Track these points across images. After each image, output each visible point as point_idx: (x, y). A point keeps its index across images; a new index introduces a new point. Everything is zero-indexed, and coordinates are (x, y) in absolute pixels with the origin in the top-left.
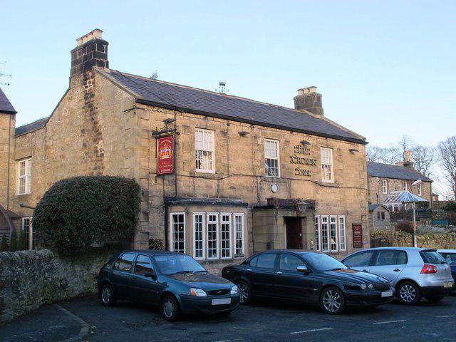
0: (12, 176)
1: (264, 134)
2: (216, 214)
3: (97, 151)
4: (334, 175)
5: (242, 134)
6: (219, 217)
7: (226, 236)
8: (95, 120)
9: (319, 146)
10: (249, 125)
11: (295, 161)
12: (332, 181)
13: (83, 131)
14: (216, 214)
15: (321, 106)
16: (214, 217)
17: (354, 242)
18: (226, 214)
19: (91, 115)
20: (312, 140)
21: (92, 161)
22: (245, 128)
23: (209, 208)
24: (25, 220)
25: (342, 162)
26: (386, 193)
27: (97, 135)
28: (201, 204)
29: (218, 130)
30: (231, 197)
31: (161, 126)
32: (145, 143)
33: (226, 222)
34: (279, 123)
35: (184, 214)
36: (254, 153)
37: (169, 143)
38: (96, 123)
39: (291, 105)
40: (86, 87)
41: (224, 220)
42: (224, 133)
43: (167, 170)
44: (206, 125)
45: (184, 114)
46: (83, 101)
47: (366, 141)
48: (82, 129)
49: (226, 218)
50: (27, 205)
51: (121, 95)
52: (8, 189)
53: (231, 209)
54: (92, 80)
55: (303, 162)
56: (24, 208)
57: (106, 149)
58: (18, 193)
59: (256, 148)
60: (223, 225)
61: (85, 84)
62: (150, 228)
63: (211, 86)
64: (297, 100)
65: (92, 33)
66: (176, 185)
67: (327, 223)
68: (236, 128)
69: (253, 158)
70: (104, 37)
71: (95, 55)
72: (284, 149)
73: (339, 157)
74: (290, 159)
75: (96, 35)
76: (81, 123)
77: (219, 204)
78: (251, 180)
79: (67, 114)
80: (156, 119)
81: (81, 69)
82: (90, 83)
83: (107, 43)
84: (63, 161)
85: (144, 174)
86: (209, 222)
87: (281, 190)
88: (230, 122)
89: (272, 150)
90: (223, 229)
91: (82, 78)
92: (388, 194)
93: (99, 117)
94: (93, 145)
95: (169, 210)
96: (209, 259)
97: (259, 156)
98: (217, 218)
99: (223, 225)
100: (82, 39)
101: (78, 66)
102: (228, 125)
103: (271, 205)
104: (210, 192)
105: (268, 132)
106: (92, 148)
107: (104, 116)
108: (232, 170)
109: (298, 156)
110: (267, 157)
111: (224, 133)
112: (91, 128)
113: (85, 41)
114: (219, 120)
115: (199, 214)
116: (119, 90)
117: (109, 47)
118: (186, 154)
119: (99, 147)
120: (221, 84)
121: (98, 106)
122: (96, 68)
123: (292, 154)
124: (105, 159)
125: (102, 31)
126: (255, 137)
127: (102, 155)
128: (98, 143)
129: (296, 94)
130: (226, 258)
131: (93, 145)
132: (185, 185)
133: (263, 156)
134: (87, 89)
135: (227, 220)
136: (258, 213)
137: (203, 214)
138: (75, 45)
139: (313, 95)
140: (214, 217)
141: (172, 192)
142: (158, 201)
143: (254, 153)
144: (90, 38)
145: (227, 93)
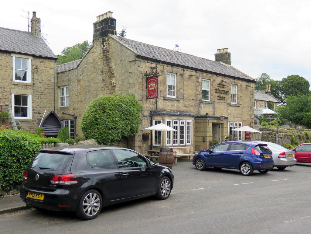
0: (56, 95)
1: (202, 76)
2: (178, 121)
3: (111, 84)
4: (238, 99)
5: (191, 76)
7: (182, 132)
8: (110, 66)
9: (230, 83)
10: (194, 71)
11: (218, 91)
13: (102, 72)
15: (230, 60)
16: (177, 122)
17: (246, 137)
18: (182, 121)
19: (107, 63)
20: (227, 80)
21: (108, 90)
22: (193, 73)
23: (174, 118)
24: (65, 121)
27: (111, 74)
28: (170, 115)
29: (178, 74)
30: (184, 112)
31: (148, 71)
32: (140, 80)
33: (182, 125)
34: (210, 70)
35: (161, 120)
37: (154, 81)
38: (110, 68)
39: (213, 58)
40: (104, 46)
41: (175, 124)
42: (182, 75)
45: (161, 64)
46: (102, 55)
48: (101, 70)
49: (182, 123)
50: (67, 113)
51: (126, 52)
52: (54, 104)
53: (186, 118)
54: (107, 42)
56: (64, 115)
57: (117, 83)
58: (60, 106)
59: (198, 84)
61: (103, 44)
63: (170, 46)
64: (217, 56)
65: (106, 14)
66: (156, 104)
68: (187, 73)
69: (196, 90)
70: (114, 16)
71: (109, 27)
72: (212, 85)
73: (240, 90)
75: (109, 15)
76: (101, 67)
77: (180, 115)
78: (194, 102)
79: (91, 61)
80: (146, 67)
81: (100, 35)
82: (106, 44)
83: (115, 20)
84: (89, 89)
87: (210, 108)
88: (185, 69)
89: (205, 86)
91: (101, 40)
93: (113, 64)
94: (108, 80)
95: (153, 118)
97: (199, 89)
99: (181, 127)
100: (99, 16)
101: (98, 33)
102: (184, 71)
103: (206, 117)
104: (174, 108)
105: (204, 75)
106: (108, 82)
107: (116, 64)
108: (185, 96)
110: (203, 89)
111: (182, 75)
112: (107, 70)
113: (102, 18)
115: (169, 120)
116: (125, 49)
117: (116, 22)
118: (161, 87)
119: (113, 82)
120: (176, 46)
121: (111, 58)
122: (110, 35)
124: (117, 89)
125: (112, 13)
126: (198, 78)
127: (115, 86)
128: (112, 79)
129: (216, 52)
130: (175, 145)
131: (108, 80)
132: (161, 104)
134: (105, 47)
135: (177, 124)
136: (199, 121)
137: (171, 121)
138: (95, 20)
139: (226, 53)
140: (177, 122)
142: (147, 113)
144: (105, 17)
145: (179, 51)
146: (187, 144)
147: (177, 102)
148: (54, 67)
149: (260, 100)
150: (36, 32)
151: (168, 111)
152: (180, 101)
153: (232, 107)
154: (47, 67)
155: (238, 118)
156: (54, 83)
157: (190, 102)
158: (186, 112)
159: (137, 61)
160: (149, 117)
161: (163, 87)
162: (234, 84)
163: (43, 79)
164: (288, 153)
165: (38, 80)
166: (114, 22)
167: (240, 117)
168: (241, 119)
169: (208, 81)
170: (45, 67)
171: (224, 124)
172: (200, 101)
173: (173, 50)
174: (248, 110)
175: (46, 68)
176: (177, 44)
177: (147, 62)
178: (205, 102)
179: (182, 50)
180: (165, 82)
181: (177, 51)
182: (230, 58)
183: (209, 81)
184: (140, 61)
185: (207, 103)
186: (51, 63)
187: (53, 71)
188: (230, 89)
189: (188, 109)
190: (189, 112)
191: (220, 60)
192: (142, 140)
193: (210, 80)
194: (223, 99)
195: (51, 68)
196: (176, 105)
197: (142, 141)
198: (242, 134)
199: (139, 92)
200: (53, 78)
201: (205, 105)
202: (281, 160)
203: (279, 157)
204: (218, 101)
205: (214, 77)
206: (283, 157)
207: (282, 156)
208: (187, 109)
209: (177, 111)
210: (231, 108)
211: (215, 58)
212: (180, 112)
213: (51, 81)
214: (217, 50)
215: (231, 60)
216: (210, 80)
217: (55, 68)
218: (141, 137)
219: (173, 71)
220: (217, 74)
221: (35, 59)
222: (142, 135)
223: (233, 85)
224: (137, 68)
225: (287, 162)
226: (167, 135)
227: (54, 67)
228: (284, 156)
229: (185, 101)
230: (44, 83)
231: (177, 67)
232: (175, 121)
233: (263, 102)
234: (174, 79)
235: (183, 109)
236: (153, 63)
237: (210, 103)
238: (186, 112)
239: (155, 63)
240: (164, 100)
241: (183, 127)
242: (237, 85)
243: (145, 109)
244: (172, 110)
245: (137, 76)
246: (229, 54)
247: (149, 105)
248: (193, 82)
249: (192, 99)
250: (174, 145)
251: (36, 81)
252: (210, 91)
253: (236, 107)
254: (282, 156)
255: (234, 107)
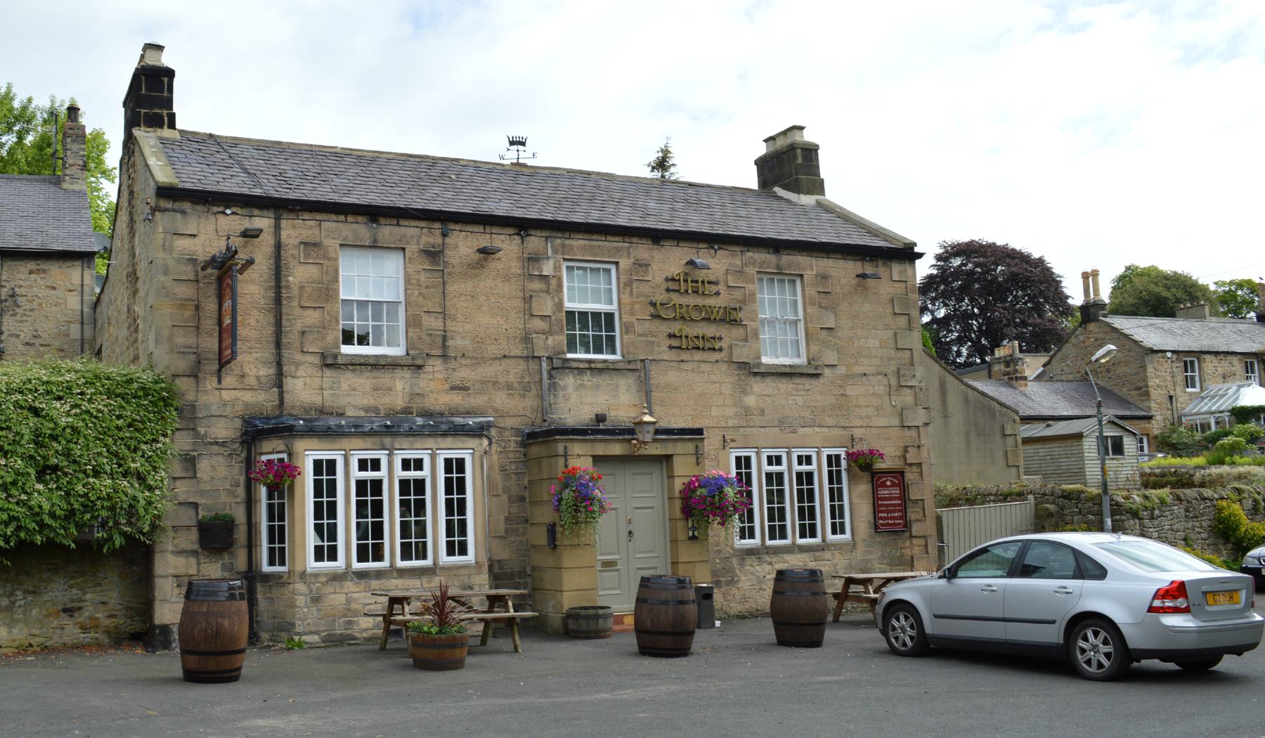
6: (390, 464)
12: (802, 361)
14: (382, 455)
20: (717, 263)
25: (833, 308)
26: (1197, 390)
29: (412, 248)
30: (454, 412)
32: (185, 291)
36: (528, 300)
39: (750, 180)
41: (770, 463)
43: (91, 357)
44: (778, 267)
47: (917, 250)
55: (695, 315)
59: (536, 285)
60: (799, 475)
62: (202, 493)
66: (280, 386)
67: (783, 468)
68: (464, 244)
72: (629, 284)
74: (652, 310)
85: (182, 364)
86: (797, 468)
88: (451, 226)
90: (800, 482)
92: (1202, 390)
96: (769, 543)
97: (545, 306)
98: (765, 461)
99: (799, 475)
108: (455, 343)
109: (677, 299)
111: (433, 255)
114: (414, 223)
115: (325, 455)
120: (512, 143)
123: (660, 297)
129: (762, 150)
133: (560, 304)
139: (792, 148)
141: (269, 405)
143: (528, 300)
145: (530, 163)
146: (831, 537)
147: (407, 374)
148: (82, 285)
149: (1216, 353)
150: (67, 172)
151: (350, 413)
152: (429, 369)
153: (769, 381)
154: (54, 288)
155: (817, 429)
156: (79, 343)
157: (490, 370)
158: (468, 413)
159: (165, 210)
160: (236, 446)
161: (317, 314)
162: (781, 276)
163: (39, 333)
164: (1204, 588)
165: (18, 336)
166: (166, 80)
167: (831, 421)
168: (840, 432)
169: (609, 271)
170: (47, 287)
171: (675, 458)
172: (550, 358)
173: (497, 161)
174: (881, 389)
175: (53, 292)
176: (517, 133)
177: (224, 213)
178: (586, 366)
179: (542, 154)
180: (327, 289)
181: (518, 164)
182: (818, 167)
183: (613, 268)
184: (183, 212)
185: (600, 366)
186: (69, 271)
187: (79, 298)
188: (750, 298)
189: (476, 401)
190: (482, 415)
191: (775, 184)
192: (196, 547)
193: (617, 263)
194: (705, 345)
195: (71, 291)
196: (399, 386)
197: (194, 553)
198: (851, 504)
199: (180, 340)
200: (78, 326)
201: (587, 379)
202: (1161, 623)
203: (1151, 609)
204: (672, 355)
205: (642, 250)
206: (1176, 610)
207: (1169, 604)
208: (472, 400)
209: (407, 411)
210: (758, 386)
211: (759, 176)
212: (427, 414)
213: (68, 335)
214: (766, 141)
215: (824, 173)
216: (801, 276)
217: (85, 288)
218: (194, 535)
219: (375, 241)
220: (657, 237)
221: (9, 263)
222: (194, 523)
223: (776, 277)
224: (164, 240)
225: (1200, 631)
226: (310, 522)
227: (82, 285)
228: (1181, 603)
229: (453, 364)
230: (42, 345)
231: (403, 222)
232: (769, 454)
233: (1235, 360)
234: (795, 295)
235: (441, 399)
236: (256, 212)
237: (621, 366)
238: (468, 413)
239: (271, 214)
240: (328, 366)
241: (810, 475)
242: (801, 276)
243: (215, 410)
244: (376, 410)
245: (166, 274)
246: (170, 73)
247: (239, 394)
248: (507, 278)
249: (499, 353)
250: (769, 543)
251: (13, 339)
252: (620, 315)
253: (796, 380)
254: (1169, 604)
255: (784, 380)
